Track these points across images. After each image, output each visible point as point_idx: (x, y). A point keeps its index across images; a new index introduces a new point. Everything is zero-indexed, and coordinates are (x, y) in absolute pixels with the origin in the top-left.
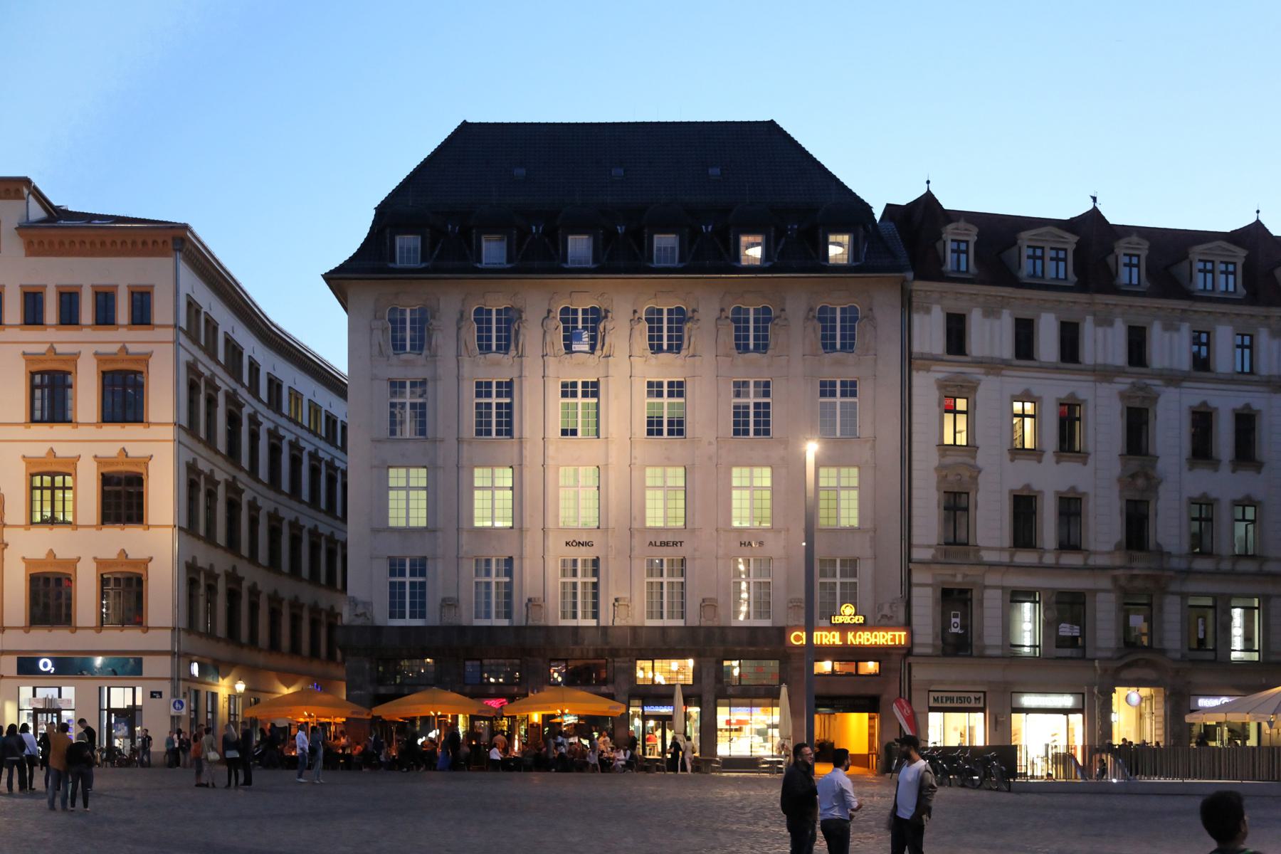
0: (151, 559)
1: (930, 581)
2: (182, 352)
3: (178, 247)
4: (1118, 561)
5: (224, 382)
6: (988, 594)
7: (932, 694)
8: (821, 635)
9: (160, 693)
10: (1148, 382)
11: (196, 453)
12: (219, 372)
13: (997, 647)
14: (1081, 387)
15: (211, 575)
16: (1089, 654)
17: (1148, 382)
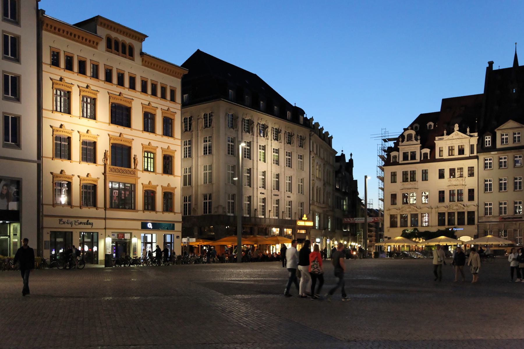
0: (176, 188)
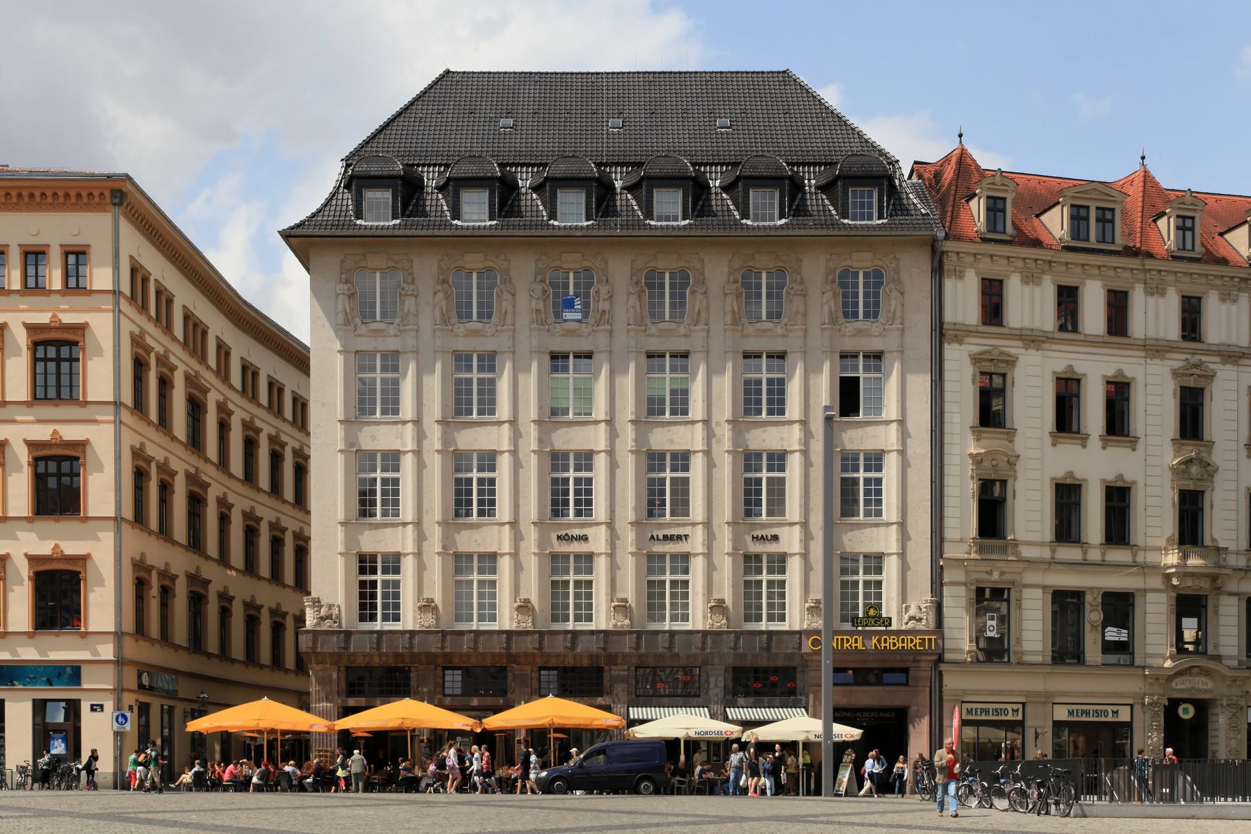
3: (117, 201)
5: (183, 364)
6: (1027, 593)
7: (965, 705)
8: (842, 639)
10: (1204, 358)
11: (145, 437)
12: (176, 349)
15: (167, 577)
16: (1138, 662)
17: (1204, 358)
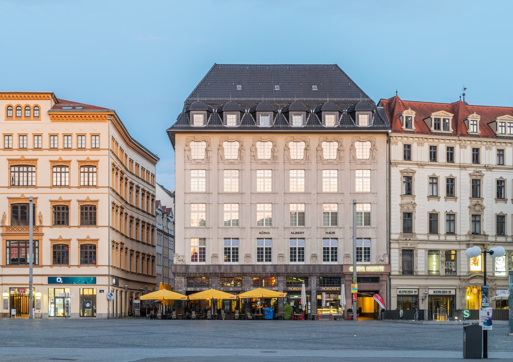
1: (397, 247)
2: (111, 159)
4: (468, 238)
6: (419, 251)
7: (398, 290)
9: (103, 291)
13: (423, 272)
14: (454, 172)
